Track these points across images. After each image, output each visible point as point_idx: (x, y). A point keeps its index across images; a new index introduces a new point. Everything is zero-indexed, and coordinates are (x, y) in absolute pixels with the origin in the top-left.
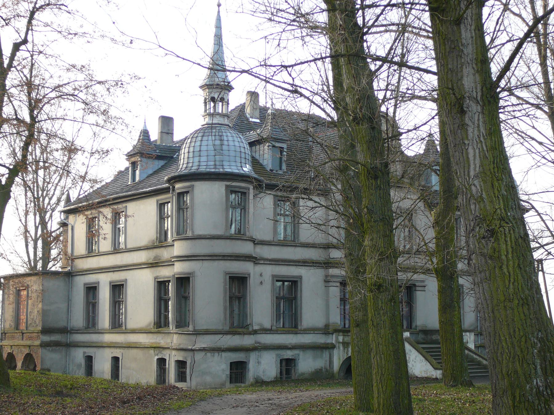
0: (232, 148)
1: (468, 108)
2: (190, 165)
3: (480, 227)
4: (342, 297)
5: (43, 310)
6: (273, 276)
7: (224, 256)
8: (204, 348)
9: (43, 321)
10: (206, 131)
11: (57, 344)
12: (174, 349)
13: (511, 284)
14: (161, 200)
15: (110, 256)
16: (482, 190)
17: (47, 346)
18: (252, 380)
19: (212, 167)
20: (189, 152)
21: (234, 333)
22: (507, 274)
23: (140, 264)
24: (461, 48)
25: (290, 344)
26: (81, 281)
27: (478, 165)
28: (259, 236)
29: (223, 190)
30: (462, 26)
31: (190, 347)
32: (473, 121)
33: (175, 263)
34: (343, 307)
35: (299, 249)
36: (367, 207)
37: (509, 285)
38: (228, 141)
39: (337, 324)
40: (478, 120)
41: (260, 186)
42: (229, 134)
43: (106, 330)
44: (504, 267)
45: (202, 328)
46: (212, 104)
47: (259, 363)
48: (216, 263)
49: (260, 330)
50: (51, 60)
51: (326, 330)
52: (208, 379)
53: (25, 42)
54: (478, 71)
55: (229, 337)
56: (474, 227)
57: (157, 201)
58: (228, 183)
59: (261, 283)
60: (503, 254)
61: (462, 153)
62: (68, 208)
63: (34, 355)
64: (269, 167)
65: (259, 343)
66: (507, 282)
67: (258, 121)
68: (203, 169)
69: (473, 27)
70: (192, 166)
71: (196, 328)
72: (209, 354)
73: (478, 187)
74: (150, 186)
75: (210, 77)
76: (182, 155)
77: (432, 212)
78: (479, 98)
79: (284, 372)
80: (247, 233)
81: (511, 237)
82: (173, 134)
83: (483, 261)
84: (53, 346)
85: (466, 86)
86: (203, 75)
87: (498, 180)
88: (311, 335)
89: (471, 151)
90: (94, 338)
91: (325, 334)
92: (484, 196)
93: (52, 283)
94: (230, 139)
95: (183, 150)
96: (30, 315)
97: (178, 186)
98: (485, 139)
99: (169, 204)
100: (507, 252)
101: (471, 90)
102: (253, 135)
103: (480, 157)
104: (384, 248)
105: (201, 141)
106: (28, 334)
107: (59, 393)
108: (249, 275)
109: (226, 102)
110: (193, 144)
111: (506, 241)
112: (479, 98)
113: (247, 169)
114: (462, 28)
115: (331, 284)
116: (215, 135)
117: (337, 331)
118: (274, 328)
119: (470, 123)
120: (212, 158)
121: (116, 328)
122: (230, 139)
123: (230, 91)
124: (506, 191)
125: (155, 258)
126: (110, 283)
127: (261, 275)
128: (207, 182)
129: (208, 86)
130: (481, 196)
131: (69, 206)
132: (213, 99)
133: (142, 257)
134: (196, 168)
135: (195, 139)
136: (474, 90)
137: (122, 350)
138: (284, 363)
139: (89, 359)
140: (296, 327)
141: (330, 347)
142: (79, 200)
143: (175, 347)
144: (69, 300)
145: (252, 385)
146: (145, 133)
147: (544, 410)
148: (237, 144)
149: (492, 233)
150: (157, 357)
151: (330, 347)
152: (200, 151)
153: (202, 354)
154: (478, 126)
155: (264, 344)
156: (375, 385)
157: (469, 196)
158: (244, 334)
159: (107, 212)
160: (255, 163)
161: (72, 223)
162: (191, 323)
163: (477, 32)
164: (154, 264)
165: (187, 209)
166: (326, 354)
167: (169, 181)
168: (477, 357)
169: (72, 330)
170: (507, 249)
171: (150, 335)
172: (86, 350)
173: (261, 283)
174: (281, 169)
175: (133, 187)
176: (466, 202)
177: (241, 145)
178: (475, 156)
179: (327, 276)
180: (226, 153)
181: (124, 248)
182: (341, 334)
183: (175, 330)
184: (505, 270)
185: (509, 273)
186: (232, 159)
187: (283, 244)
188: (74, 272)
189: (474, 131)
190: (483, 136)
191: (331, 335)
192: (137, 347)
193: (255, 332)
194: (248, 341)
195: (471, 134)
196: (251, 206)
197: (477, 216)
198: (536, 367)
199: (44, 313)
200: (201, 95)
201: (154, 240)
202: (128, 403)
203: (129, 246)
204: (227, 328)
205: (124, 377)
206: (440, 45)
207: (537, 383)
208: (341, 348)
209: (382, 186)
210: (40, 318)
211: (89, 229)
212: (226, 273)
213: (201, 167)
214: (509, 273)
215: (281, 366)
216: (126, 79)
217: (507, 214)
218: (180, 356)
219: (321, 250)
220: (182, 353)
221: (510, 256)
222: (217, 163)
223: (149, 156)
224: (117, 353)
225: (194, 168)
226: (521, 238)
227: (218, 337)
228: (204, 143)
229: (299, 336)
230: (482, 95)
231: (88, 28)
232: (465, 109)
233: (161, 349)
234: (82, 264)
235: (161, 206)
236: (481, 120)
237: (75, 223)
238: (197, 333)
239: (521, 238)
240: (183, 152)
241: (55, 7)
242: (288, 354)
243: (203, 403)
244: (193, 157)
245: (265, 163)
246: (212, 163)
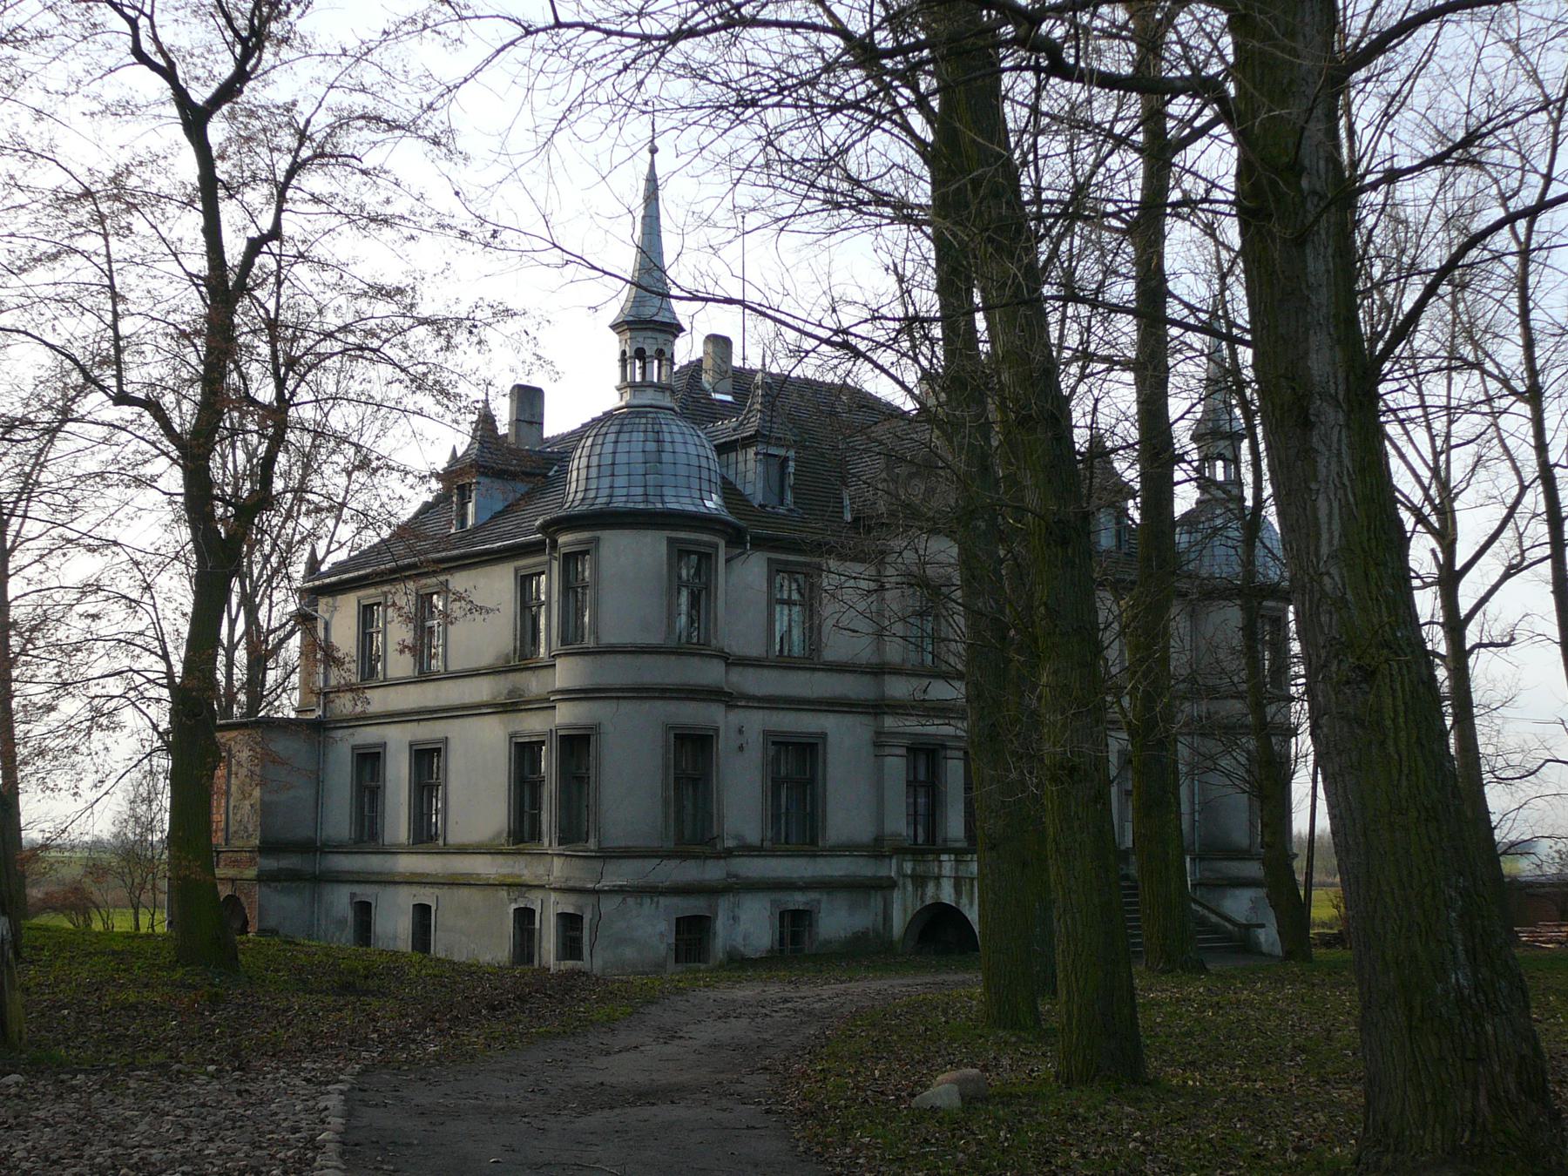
0: (682, 459)
1: (1317, 416)
2: (592, 494)
3: (1340, 661)
4: (911, 778)
5: (263, 802)
6: (767, 734)
7: (664, 690)
8: (621, 886)
9: (264, 826)
10: (626, 421)
11: (294, 876)
12: (555, 889)
13: (1404, 778)
14: (525, 567)
15: (411, 688)
16: (1344, 586)
17: (273, 881)
18: (721, 955)
19: (640, 499)
20: (588, 467)
21: (683, 856)
22: (1396, 757)
23: (479, 706)
24: (1306, 293)
25: (802, 878)
26: (344, 744)
27: (1336, 534)
28: (737, 647)
29: (663, 548)
30: (1309, 250)
31: (590, 886)
32: (1328, 442)
33: (558, 705)
34: (912, 800)
35: (819, 676)
36: (1045, 604)
37: (1399, 780)
38: (672, 442)
39: (900, 835)
40: (1339, 441)
41: (736, 538)
42: (675, 429)
43: (399, 846)
44: (1390, 742)
45: (615, 844)
46: (638, 364)
47: (735, 919)
48: (646, 706)
49: (739, 848)
50: (330, 277)
51: (878, 849)
52: (629, 953)
53: (276, 233)
54: (1339, 341)
55: (673, 863)
56: (1326, 661)
57: (516, 570)
58: (674, 534)
59: (741, 748)
60: (1386, 716)
61: (1305, 509)
62: (311, 584)
63: (243, 899)
64: (758, 499)
65: (736, 876)
66: (1394, 772)
67: (729, 398)
68: (619, 503)
69: (1330, 251)
70: (596, 497)
71: (605, 844)
72: (630, 901)
73: (1337, 578)
74: (500, 539)
75: (637, 302)
76: (575, 474)
77: (1122, 602)
78: (1341, 397)
79: (788, 940)
80: (713, 642)
81: (1402, 683)
82: (542, 424)
83: (1345, 729)
84: (286, 880)
85: (1314, 372)
86: (615, 299)
87: (1377, 564)
88: (845, 859)
89: (1323, 506)
90: (375, 862)
91: (876, 857)
92: (1349, 596)
93: (282, 746)
94: (678, 438)
95: (576, 462)
96: (235, 814)
97: (563, 539)
98: (1351, 480)
99: (543, 577)
100: (1395, 711)
101: (1324, 379)
102: (726, 428)
103: (1341, 518)
104: (1082, 689)
105: (616, 442)
106: (230, 855)
107: (346, 988)
108: (717, 730)
109: (667, 359)
110: (597, 449)
111: (1394, 691)
112: (1341, 397)
113: (713, 503)
114: (1308, 251)
115: (887, 751)
116: (645, 431)
117: (900, 851)
118: (767, 844)
119: (1322, 448)
120: (639, 480)
121: (422, 842)
122: (678, 438)
123: (676, 336)
124: (1393, 587)
125: (511, 693)
126: (411, 746)
127: (740, 731)
128: (627, 532)
129: (628, 325)
130: (1343, 597)
131: (313, 580)
132: (640, 354)
133: (482, 690)
134: (604, 500)
135: (601, 437)
136: (1332, 381)
137: (436, 891)
138: (787, 920)
139: (364, 910)
140: (814, 842)
141: (885, 886)
142: (339, 567)
143: (557, 886)
144: (318, 780)
145: (721, 966)
146: (486, 420)
147: (1472, 1036)
148: (692, 449)
149: (1369, 675)
150: (514, 906)
151: (885, 886)
152: (613, 464)
153: (618, 899)
154: (1339, 454)
155: (747, 878)
156: (1060, 976)
157: (1317, 595)
158: (707, 858)
159: (404, 596)
160: (730, 492)
161: (327, 616)
162: (592, 834)
163: (1337, 260)
164: (509, 706)
165: (584, 588)
166: (877, 901)
167: (544, 528)
168: (1199, 909)
169: (325, 845)
170: (1395, 706)
171: (500, 859)
172: (357, 889)
173: (741, 748)
174: (782, 504)
175: (461, 539)
176: (1311, 608)
177: (701, 451)
178: (1330, 515)
179: (878, 733)
180: (668, 469)
181: (442, 670)
182: (909, 857)
183: (556, 848)
184: (1391, 749)
185: (1400, 755)
186: (682, 481)
187: (785, 663)
188: (329, 722)
189: (1329, 463)
190: (1349, 475)
191: (887, 860)
192: (470, 884)
193: (729, 853)
194: (713, 872)
195: (1324, 470)
196: (721, 580)
197: (1334, 638)
198: (1455, 947)
199: (266, 810)
200: (613, 345)
201: (507, 655)
202: (502, 1009)
203: (454, 666)
204: (670, 845)
205: (440, 945)
206: (1260, 286)
207: (1457, 979)
208: (910, 888)
209: (1077, 561)
210: (256, 819)
211: (365, 627)
212: (670, 728)
213: (614, 499)
214: (1400, 755)
215: (782, 925)
216: (483, 315)
217: (1394, 634)
218: (568, 905)
219: (866, 679)
220: (573, 898)
221: (1401, 720)
222: (651, 491)
223: (500, 474)
224: (426, 896)
225: (599, 501)
226: (1423, 683)
227: (649, 864)
228: (622, 447)
229: (821, 861)
230: (1348, 390)
231: (400, 206)
232: (1313, 419)
233: (524, 889)
234: (345, 705)
235: (524, 582)
236: (1345, 441)
237: (331, 617)
238: (607, 855)
239: (1423, 683)
240: (575, 466)
241: (333, 161)
242: (798, 900)
243: (653, 1008)
244: (598, 477)
245: (748, 490)
246: (640, 491)
